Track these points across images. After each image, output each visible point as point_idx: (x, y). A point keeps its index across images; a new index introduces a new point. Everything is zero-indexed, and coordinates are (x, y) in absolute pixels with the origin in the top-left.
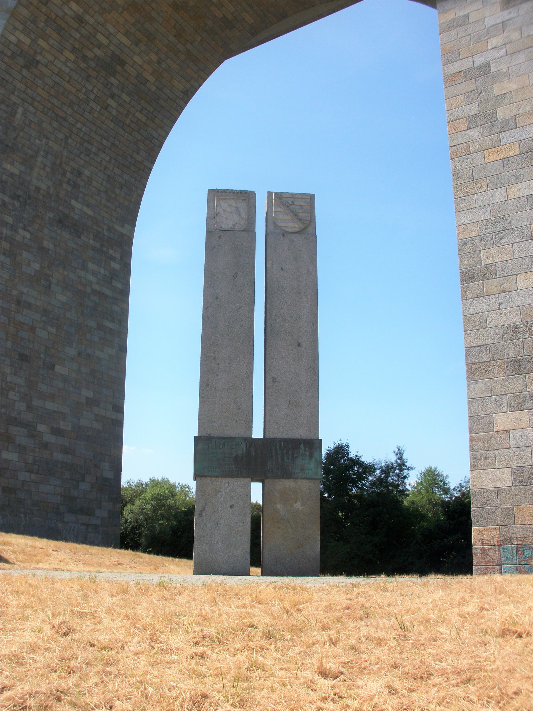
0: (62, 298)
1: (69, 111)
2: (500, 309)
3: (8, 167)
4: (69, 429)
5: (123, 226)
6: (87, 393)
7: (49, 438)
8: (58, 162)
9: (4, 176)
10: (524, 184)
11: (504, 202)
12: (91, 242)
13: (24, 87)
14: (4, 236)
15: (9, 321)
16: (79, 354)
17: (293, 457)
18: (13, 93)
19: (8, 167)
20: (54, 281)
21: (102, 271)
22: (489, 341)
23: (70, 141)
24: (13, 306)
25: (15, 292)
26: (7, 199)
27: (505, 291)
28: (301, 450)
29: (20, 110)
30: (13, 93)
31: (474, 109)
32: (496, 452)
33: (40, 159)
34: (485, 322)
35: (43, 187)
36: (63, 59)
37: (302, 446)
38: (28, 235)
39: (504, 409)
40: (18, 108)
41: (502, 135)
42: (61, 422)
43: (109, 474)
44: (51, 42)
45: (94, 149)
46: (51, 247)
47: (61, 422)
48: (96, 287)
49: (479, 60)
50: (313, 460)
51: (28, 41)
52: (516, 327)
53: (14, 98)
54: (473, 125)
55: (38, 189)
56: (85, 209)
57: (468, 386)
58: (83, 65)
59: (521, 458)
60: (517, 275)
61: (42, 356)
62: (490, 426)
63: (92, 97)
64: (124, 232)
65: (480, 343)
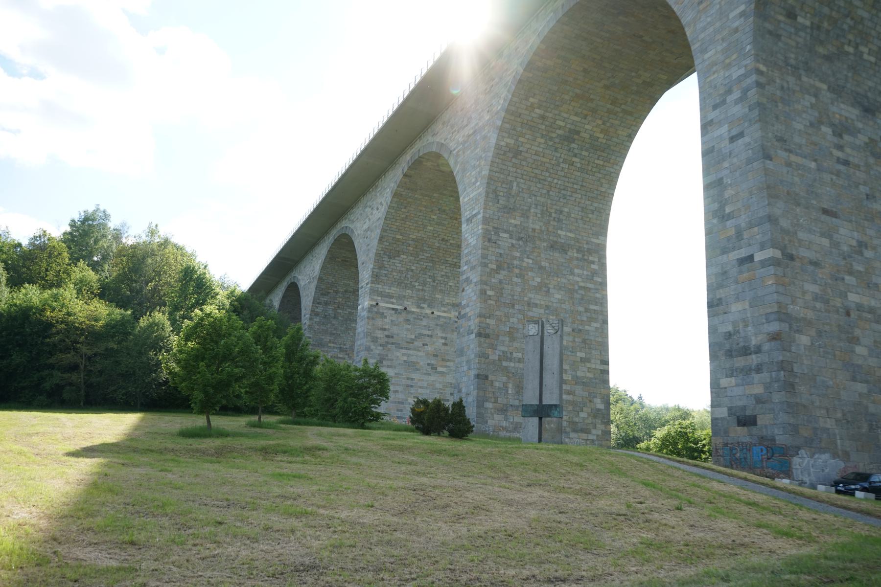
1: (547, 174)
3: (513, 221)
4: (570, 379)
8: (545, 208)
10: (736, 252)
12: (575, 255)
19: (513, 221)
20: (551, 286)
23: (551, 193)
25: (526, 299)
26: (514, 242)
29: (515, 184)
30: (509, 175)
33: (532, 210)
35: (537, 227)
38: (531, 261)
48: (582, 284)
51: (512, 142)
53: (510, 178)
55: (534, 230)
56: (569, 234)
58: (551, 143)
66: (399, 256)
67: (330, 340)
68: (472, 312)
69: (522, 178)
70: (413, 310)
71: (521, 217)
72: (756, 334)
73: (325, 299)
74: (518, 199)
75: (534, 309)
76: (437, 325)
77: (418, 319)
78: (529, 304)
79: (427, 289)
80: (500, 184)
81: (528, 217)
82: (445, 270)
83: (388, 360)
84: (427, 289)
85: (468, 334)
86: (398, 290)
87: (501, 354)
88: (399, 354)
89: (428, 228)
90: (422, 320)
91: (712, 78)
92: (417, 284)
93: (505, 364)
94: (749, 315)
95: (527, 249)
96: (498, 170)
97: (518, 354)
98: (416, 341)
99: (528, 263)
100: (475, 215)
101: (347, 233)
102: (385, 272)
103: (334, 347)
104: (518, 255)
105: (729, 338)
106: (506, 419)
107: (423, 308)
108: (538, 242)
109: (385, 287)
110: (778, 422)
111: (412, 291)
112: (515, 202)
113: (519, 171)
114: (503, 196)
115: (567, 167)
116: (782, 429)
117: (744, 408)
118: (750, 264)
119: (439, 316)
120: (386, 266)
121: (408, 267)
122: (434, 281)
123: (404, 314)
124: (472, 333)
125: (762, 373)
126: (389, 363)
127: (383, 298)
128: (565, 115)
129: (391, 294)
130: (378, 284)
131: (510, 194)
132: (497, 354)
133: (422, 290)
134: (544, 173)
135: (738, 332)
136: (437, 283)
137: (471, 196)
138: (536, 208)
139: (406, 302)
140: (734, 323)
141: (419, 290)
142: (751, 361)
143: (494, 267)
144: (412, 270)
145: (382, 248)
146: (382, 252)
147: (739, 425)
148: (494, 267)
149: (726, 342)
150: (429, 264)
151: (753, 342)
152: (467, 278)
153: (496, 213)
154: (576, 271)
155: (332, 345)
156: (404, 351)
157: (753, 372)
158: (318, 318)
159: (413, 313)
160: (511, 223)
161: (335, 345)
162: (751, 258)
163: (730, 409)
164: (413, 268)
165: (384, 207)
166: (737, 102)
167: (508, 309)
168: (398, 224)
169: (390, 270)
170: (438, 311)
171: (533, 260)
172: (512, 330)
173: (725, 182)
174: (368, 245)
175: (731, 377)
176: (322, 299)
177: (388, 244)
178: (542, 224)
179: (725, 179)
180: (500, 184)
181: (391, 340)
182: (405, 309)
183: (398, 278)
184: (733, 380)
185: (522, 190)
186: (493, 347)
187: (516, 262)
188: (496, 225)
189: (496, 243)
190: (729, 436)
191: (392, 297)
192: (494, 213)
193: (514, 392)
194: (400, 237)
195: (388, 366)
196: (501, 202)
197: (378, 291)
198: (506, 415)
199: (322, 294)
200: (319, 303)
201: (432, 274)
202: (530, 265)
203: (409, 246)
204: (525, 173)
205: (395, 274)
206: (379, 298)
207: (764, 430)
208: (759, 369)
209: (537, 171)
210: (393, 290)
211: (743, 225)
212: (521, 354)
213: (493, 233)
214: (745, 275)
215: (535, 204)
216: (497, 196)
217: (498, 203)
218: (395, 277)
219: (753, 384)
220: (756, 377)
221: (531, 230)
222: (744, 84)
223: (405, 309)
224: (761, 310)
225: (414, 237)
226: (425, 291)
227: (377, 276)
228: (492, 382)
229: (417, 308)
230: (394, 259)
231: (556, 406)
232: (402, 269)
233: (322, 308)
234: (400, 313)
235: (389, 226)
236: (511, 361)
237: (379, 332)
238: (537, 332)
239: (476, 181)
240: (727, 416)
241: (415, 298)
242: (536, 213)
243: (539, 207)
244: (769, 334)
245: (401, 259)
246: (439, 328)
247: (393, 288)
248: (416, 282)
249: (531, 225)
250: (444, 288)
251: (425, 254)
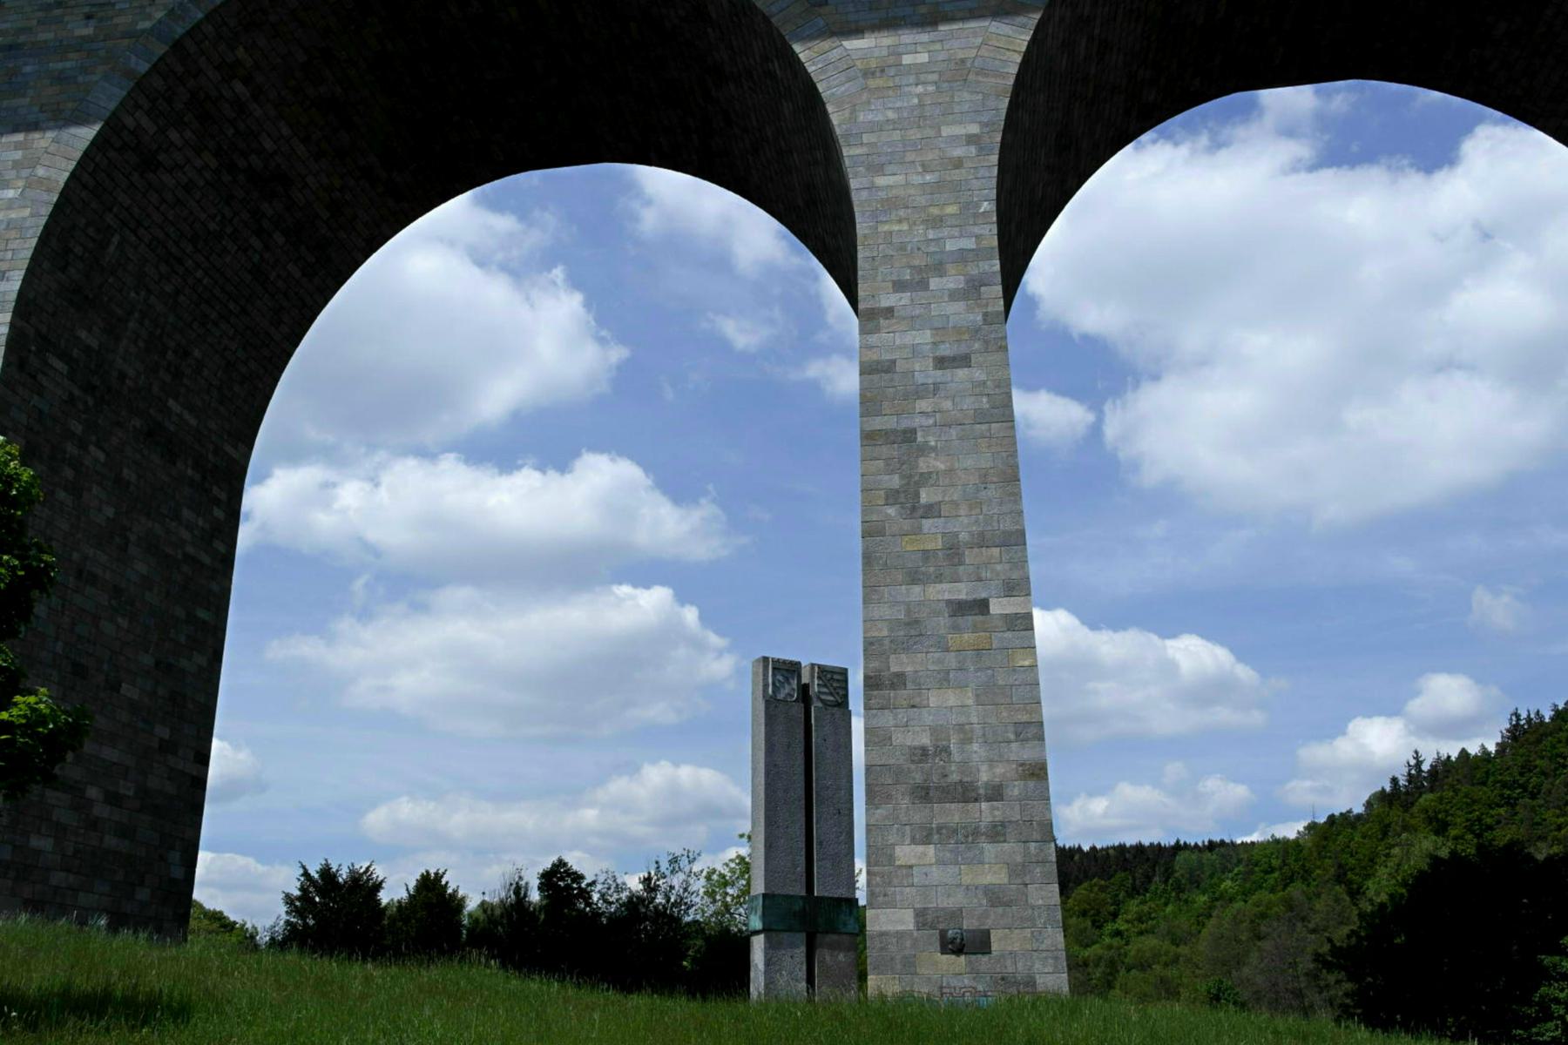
0: (142, 568)
1: (189, 249)
2: (907, 726)
3: (83, 334)
4: (131, 793)
5: (236, 448)
6: (163, 732)
7: (101, 810)
8: (158, 332)
9: (76, 351)
10: (945, 586)
11: (920, 603)
12: (190, 472)
13: (129, 202)
14: (68, 456)
15: (63, 606)
16: (157, 664)
18: (110, 210)
19: (83, 334)
20: (133, 538)
21: (200, 523)
22: (892, 761)
23: (182, 298)
24: (71, 579)
25: (76, 556)
26: (77, 392)
27: (913, 706)
29: (116, 239)
30: (110, 210)
31: (895, 481)
32: (897, 889)
33: (131, 325)
34: (890, 738)
35: (131, 372)
36: (198, 163)
37: (843, 903)
38: (102, 457)
39: (908, 842)
40: (113, 235)
41: (924, 521)
42: (122, 782)
43: (178, 873)
44: (188, 134)
45: (214, 315)
46: (133, 478)
47: (122, 782)
48: (190, 550)
49: (905, 423)
51: (152, 129)
52: (924, 749)
53: (109, 219)
54: (891, 501)
55: (122, 376)
56: (187, 416)
57: (867, 810)
58: (226, 178)
59: (925, 899)
60: (929, 689)
61: (105, 667)
62: (891, 858)
63: (229, 230)
64: (235, 455)
65: (882, 762)
69: (135, 232)
72: (991, 762)
78: (79, 574)
91: (896, 228)
94: (974, 720)
104: (78, 429)
105: (920, 761)
110: (1043, 947)
116: (1050, 961)
117: (956, 914)
118: (980, 618)
125: (1005, 841)
128: (286, 131)
135: (946, 750)
140: (935, 731)
142: (977, 815)
147: (945, 949)
149: (913, 767)
151: (984, 777)
154: (186, 513)
157: (1277, 866)
162: (982, 606)
163: (920, 914)
166: (954, 296)
171: (108, 454)
173: (920, 439)
175: (924, 843)
179: (919, 434)
184: (931, 849)
187: (71, 449)
189: (34, 377)
190: (916, 974)
207: (1009, 963)
208: (997, 833)
211: (964, 536)
213: (33, 348)
214: (966, 636)
219: (982, 863)
220: (990, 850)
222: (973, 270)
224: (1005, 714)
240: (911, 927)
244: (1022, 765)
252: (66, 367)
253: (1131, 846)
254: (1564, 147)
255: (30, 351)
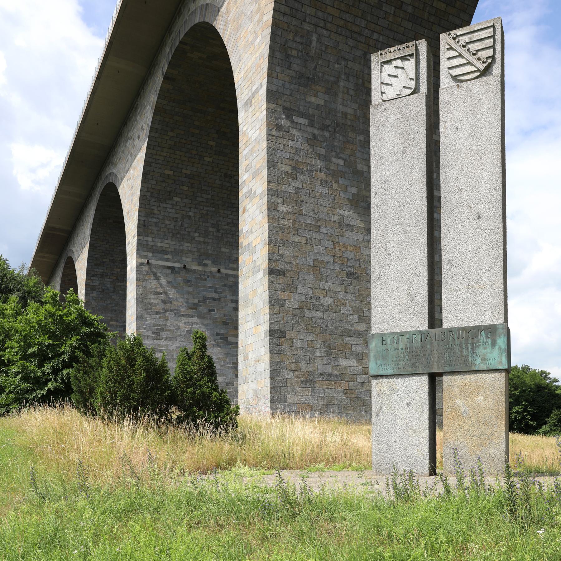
1: (363, 23)
3: (313, 99)
17: (473, 347)
19: (313, 99)
26: (316, 132)
28: (482, 338)
29: (314, 38)
30: (305, 21)
33: (342, 84)
35: (350, 111)
37: (483, 333)
38: (341, 162)
50: (497, 347)
53: (306, 27)
55: (345, 115)
66: (171, 199)
67: (111, 318)
68: (258, 239)
70: (193, 268)
71: (326, 93)
73: (101, 271)
74: (320, 62)
75: (348, 234)
76: (225, 286)
77: (201, 279)
78: (340, 224)
79: (211, 241)
80: (291, 36)
81: (335, 95)
82: (231, 217)
83: (166, 331)
84: (211, 241)
85: (254, 273)
86: (173, 243)
87: (303, 298)
88: (180, 324)
89: (206, 159)
90: (205, 280)
92: (196, 235)
93: (308, 314)
95: (336, 144)
96: (288, 10)
97: (327, 299)
98: (201, 306)
99: (338, 165)
100: (257, 91)
101: (111, 181)
102: (154, 220)
103: (117, 325)
106: (313, 393)
107: (206, 265)
108: (351, 134)
109: (157, 240)
111: (191, 243)
112: (315, 69)
113: (320, 14)
114: (298, 57)
115: (392, 12)
119: (227, 275)
120: (155, 212)
121: (184, 213)
122: (218, 231)
123: (183, 273)
124: (259, 270)
126: (169, 334)
127: (155, 254)
129: (164, 249)
130: (148, 236)
131: (307, 54)
132: (297, 299)
133: (204, 242)
134: (358, 21)
136: (222, 233)
137: (249, 64)
138: (348, 80)
139: (184, 259)
141: (200, 242)
143: (288, 169)
144: (190, 217)
145: (148, 188)
146: (149, 194)
148: (288, 169)
150: (211, 209)
152: (248, 191)
153: (287, 85)
155: (114, 323)
156: (185, 319)
158: (94, 292)
159: (194, 271)
160: (310, 102)
161: (118, 324)
164: (190, 214)
165: (145, 131)
167: (310, 233)
168: (165, 154)
169: (161, 217)
170: (226, 269)
171: (345, 160)
172: (317, 264)
174: (132, 188)
176: (97, 270)
177: (154, 182)
178: (356, 106)
180: (291, 36)
181: (168, 307)
182: (184, 267)
183: (172, 227)
185: (326, 48)
186: (290, 288)
188: (288, 105)
191: (166, 252)
192: (283, 85)
193: (323, 354)
194: (171, 173)
195: (167, 339)
196: (294, 66)
197: (147, 245)
198: (313, 389)
199: (96, 265)
200: (93, 275)
201: (215, 222)
202: (340, 168)
203: (183, 185)
204: (330, 19)
205: (167, 222)
206: (150, 254)
209: (347, 16)
210: (167, 244)
212: (332, 299)
215: (345, 73)
216: (288, 56)
217: (289, 67)
218: (168, 226)
221: (340, 115)
223: (184, 267)
225: (189, 172)
226: (208, 243)
227: (145, 226)
228: (291, 339)
229: (200, 265)
230: (165, 203)
231: (491, 330)
232: (176, 216)
233: (98, 282)
234: (178, 272)
235: (154, 157)
236: (318, 310)
237: (154, 296)
238: (412, 84)
239: (255, 39)
241: (196, 253)
242: (348, 89)
243: (351, 78)
245: (174, 203)
246: (227, 289)
247: (166, 241)
248: (195, 232)
249: (341, 107)
250: (231, 240)
251: (204, 195)
252: (307, 121)
253: (516, 368)
254: (480, 7)
255: (282, 119)
